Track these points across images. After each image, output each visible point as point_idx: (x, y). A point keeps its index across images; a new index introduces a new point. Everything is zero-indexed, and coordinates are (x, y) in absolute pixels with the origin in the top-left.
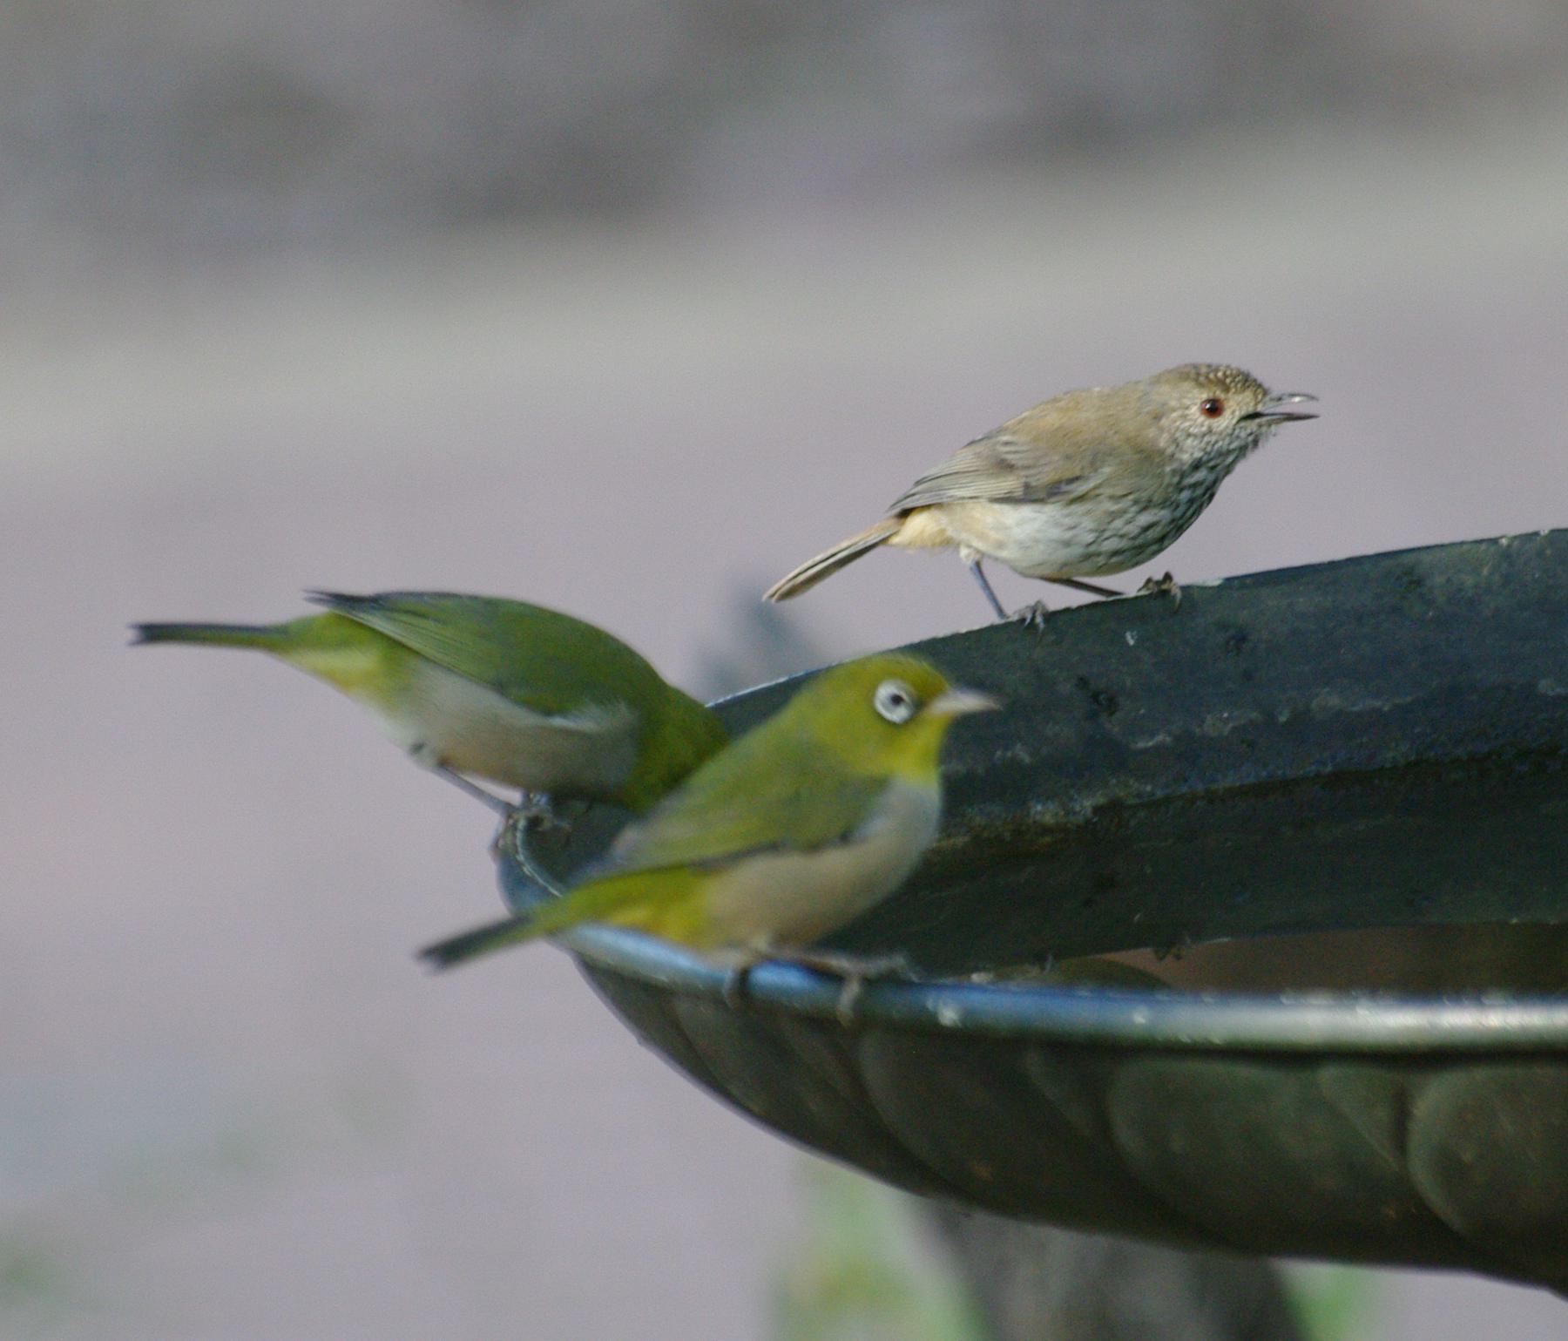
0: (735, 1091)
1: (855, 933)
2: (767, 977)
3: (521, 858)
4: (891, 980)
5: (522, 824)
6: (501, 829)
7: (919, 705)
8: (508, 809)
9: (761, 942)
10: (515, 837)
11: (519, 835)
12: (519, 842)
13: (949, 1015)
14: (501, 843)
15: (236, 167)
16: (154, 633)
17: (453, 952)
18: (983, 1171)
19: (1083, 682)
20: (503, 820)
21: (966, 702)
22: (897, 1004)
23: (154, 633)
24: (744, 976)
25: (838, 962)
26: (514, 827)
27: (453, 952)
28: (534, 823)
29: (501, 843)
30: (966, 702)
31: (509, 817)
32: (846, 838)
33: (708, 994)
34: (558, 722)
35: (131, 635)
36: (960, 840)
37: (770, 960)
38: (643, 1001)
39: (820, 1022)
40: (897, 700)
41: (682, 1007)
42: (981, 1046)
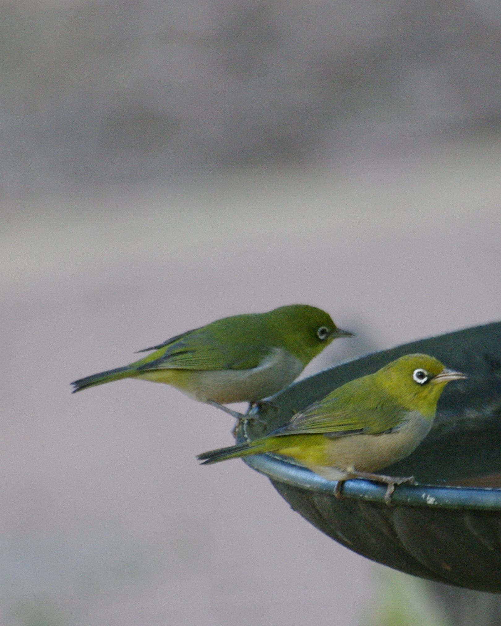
0: (340, 534)
1: (393, 467)
2: (350, 485)
3: (246, 436)
4: (407, 485)
5: (246, 422)
6: (237, 424)
7: (431, 378)
8: (240, 416)
9: (350, 469)
10: (243, 427)
11: (245, 426)
12: (245, 429)
13: (431, 501)
14: (237, 430)
15: (125, 144)
16: (82, 384)
17: (211, 457)
18: (447, 567)
19: (486, 357)
20: (238, 421)
21: (452, 375)
22: (409, 497)
23: (82, 384)
24: (342, 484)
25: (384, 478)
26: (243, 423)
27: (211, 457)
28: (250, 422)
29: (237, 430)
30: (452, 375)
31: (240, 419)
32: (390, 431)
33: (324, 492)
34: (256, 370)
35: (72, 388)
36: (437, 425)
37: (353, 478)
38: (299, 497)
39: (375, 505)
40: (421, 376)
41: (316, 499)
42: (441, 512)
